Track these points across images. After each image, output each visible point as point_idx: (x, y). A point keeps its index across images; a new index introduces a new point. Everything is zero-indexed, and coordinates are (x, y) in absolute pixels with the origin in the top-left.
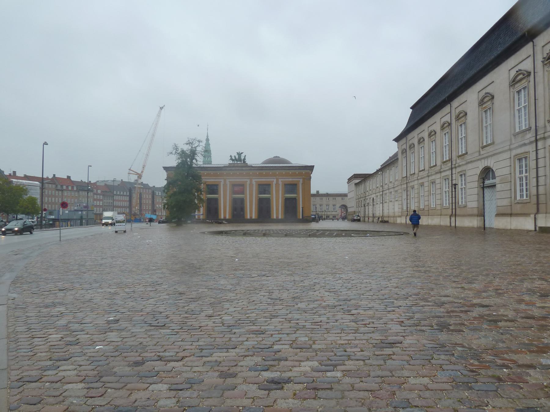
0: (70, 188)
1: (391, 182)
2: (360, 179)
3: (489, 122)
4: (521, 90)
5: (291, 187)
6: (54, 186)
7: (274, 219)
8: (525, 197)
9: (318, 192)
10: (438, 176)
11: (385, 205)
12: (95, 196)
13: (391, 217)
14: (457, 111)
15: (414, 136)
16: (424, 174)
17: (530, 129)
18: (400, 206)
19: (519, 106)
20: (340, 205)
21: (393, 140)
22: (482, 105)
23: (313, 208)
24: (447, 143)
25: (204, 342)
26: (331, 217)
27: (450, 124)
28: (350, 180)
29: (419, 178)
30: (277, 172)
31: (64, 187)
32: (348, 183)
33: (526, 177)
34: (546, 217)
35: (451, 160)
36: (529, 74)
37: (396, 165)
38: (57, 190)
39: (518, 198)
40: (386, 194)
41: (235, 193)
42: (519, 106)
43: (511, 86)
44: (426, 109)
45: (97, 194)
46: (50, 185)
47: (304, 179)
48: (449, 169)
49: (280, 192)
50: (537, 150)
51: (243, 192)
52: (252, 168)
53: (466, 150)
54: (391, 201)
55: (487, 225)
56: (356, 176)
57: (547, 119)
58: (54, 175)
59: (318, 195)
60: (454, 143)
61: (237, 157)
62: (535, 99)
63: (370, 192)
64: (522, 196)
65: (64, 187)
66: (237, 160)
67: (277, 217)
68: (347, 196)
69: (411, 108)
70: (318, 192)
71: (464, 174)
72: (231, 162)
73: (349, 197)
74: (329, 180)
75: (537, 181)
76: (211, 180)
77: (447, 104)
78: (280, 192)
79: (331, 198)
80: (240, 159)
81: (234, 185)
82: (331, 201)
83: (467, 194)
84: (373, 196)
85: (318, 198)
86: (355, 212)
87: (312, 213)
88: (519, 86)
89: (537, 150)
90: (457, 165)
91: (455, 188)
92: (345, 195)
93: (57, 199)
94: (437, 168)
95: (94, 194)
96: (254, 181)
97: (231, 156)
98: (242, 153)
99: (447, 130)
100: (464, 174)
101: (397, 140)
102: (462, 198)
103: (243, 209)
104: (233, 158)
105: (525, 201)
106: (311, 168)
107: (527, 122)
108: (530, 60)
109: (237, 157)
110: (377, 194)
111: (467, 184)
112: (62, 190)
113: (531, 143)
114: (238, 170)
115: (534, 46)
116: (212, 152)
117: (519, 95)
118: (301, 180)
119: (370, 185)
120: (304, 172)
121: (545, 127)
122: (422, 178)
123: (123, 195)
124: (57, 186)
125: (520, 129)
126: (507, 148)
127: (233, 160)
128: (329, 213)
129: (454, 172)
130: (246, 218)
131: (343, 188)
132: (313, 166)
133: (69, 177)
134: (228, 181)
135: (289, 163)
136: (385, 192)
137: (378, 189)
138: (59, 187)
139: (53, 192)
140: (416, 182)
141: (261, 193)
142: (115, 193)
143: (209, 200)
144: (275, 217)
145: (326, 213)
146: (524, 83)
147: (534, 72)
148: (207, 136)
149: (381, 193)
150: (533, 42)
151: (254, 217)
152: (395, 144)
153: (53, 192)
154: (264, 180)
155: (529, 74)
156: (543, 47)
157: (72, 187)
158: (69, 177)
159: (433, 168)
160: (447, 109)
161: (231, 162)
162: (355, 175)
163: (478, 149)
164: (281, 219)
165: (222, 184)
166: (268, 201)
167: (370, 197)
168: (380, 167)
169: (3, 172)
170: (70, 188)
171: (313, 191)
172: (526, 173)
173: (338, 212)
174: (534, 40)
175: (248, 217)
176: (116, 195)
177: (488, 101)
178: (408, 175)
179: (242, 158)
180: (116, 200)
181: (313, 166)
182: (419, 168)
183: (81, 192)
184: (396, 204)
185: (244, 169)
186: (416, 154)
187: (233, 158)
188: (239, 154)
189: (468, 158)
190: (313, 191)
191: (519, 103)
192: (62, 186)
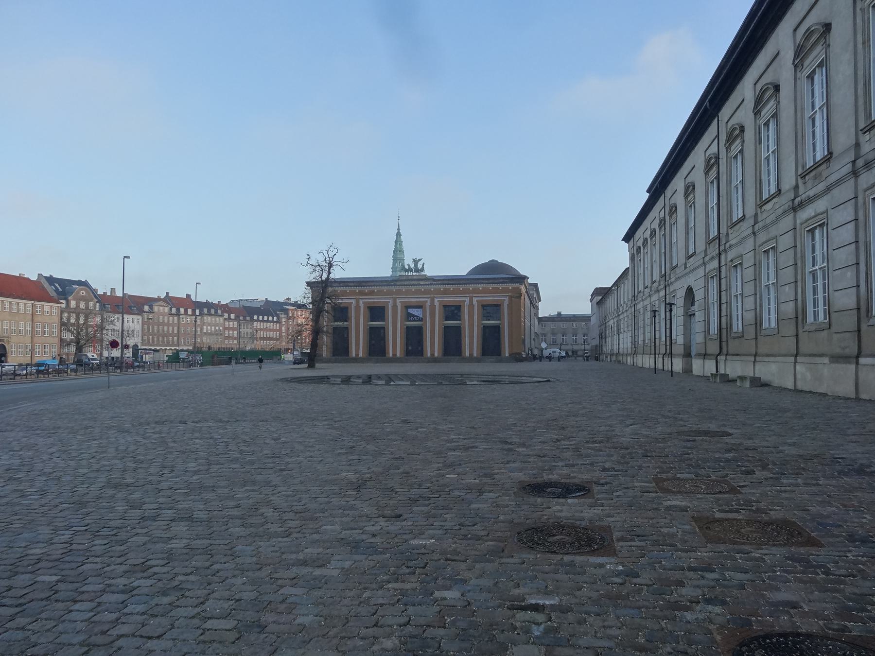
2: (601, 295)
11: (621, 336)
12: (227, 323)
25: (703, 577)
31: (182, 310)
32: (591, 300)
34: (726, 360)
35: (719, 237)
41: (487, 317)
47: (511, 298)
49: (476, 317)
51: (346, 319)
52: (433, 280)
58: (167, 293)
59: (559, 318)
61: (412, 266)
65: (182, 310)
78: (476, 317)
81: (484, 306)
91: (671, 310)
93: (171, 328)
96: (436, 300)
98: (420, 260)
101: (627, 238)
103: (420, 342)
109: (412, 266)
118: (507, 299)
128: (575, 347)
131: (585, 308)
136: (621, 317)
139: (166, 318)
141: (447, 319)
143: (335, 329)
148: (398, 229)
151: (475, 355)
153: (166, 318)
154: (450, 299)
162: (596, 289)
166: (458, 330)
169: (501, 283)
177: (768, 100)
183: (205, 318)
189: (678, 271)
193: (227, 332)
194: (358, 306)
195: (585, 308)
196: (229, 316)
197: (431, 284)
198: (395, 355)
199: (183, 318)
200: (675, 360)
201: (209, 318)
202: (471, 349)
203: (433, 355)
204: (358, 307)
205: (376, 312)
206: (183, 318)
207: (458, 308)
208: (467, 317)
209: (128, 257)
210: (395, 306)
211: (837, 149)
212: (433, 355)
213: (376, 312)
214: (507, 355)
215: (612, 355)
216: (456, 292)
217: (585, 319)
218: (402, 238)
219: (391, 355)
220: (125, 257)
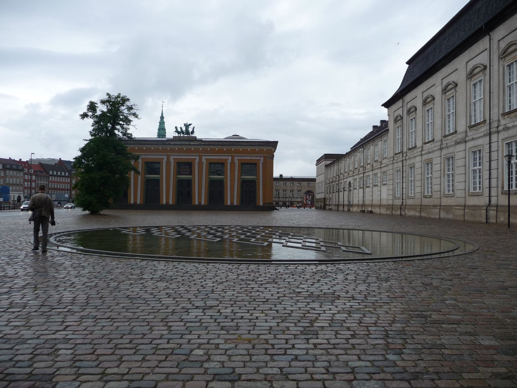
2: (330, 160)
3: (452, 111)
4: (512, 63)
5: (249, 167)
7: (228, 206)
8: (478, 190)
9: (281, 176)
10: (461, 147)
11: (367, 190)
12: (26, 176)
13: (376, 206)
14: (409, 107)
15: (416, 97)
16: (435, 146)
17: (485, 121)
18: (391, 192)
19: (510, 82)
20: (306, 191)
21: (383, 105)
22: (446, 93)
23: (275, 193)
24: (400, 136)
26: (281, 203)
27: (402, 118)
28: (319, 161)
29: (423, 152)
32: (317, 165)
33: (480, 170)
36: (485, 68)
37: (384, 138)
39: (472, 190)
40: (341, 183)
42: (510, 82)
43: (469, 78)
44: (425, 65)
47: (265, 158)
48: (485, 135)
49: (236, 173)
50: (490, 143)
53: (415, 144)
54: (377, 185)
55: (441, 217)
56: (327, 157)
57: (500, 113)
59: (281, 178)
60: (405, 137)
61: (184, 129)
62: (490, 92)
63: (346, 174)
64: (475, 189)
66: (183, 133)
67: (232, 203)
69: (407, 63)
70: (281, 176)
71: (431, 163)
72: (177, 135)
73: (317, 182)
75: (490, 174)
76: (152, 157)
77: (486, 35)
78: (236, 173)
79: (296, 183)
80: (187, 132)
83: (433, 183)
84: (349, 179)
85: (282, 183)
87: (274, 199)
88: (475, 80)
89: (490, 143)
90: (501, 128)
92: (313, 180)
94: (459, 137)
95: (25, 174)
97: (176, 128)
98: (190, 125)
99: (399, 123)
100: (452, 158)
101: (387, 105)
102: (428, 188)
104: (179, 130)
105: (479, 194)
107: (482, 115)
108: (486, 53)
109: (184, 129)
110: (355, 177)
111: (434, 173)
113: (485, 135)
115: (490, 39)
116: (166, 131)
117: (510, 69)
118: (262, 159)
119: (343, 165)
120: (265, 149)
121: (499, 120)
122: (429, 153)
123: (60, 176)
125: (510, 108)
126: (379, 166)
127: (179, 133)
128: (293, 200)
129: (404, 164)
130: (193, 204)
132: (277, 142)
133: (60, 159)
137: (356, 171)
140: (418, 159)
141: (213, 173)
142: (51, 173)
144: (229, 203)
145: (290, 200)
146: (480, 77)
147: (490, 65)
148: (162, 114)
149: (337, 182)
150: (490, 36)
151: (171, 202)
152: (385, 110)
155: (485, 68)
156: (499, 41)
159: (450, 137)
160: (483, 44)
161: (177, 135)
162: (325, 155)
163: (440, 139)
164: (140, 205)
167: (345, 180)
168: (350, 150)
171: (276, 175)
172: (480, 166)
174: (491, 34)
175: (229, 203)
176: (52, 176)
178: (405, 150)
179: (190, 130)
180: (68, 183)
181: (277, 142)
182: (423, 138)
183: (7, 172)
184: (384, 189)
185: (192, 143)
186: (419, 121)
187: (179, 130)
188: (187, 126)
190: (276, 175)
191: (510, 79)
193: (26, 183)
195: (384, 114)
197: (200, 145)
200: (500, 214)
201: (11, 172)
204: (168, 163)
205: (152, 167)
207: (223, 164)
208: (229, 172)
210: (168, 163)
211: (436, 140)
213: (217, 167)
214: (261, 204)
215: (344, 205)
216: (221, 152)
218: (165, 120)
219: (132, 202)
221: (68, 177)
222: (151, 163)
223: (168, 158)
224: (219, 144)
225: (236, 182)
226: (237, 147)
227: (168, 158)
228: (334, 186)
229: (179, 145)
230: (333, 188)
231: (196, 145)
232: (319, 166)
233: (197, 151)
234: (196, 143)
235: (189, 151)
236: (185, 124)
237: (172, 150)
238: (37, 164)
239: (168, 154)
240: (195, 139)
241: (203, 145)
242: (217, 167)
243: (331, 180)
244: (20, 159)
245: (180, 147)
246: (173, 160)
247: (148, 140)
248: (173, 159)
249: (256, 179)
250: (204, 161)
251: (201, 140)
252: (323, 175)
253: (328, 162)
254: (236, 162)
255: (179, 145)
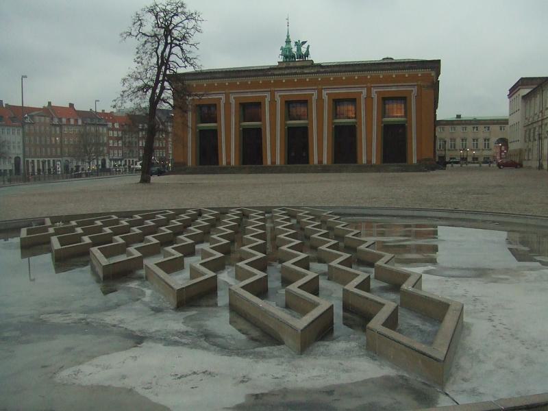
0: (72, 122)
1: (535, 115)
6: (48, 119)
7: (316, 166)
12: (111, 132)
28: (513, 90)
30: (369, 75)
31: (64, 120)
32: (510, 96)
38: (53, 125)
45: (113, 129)
46: (43, 119)
47: (420, 87)
49: (375, 113)
51: (214, 119)
56: (524, 82)
58: (50, 103)
59: (458, 122)
65: (64, 120)
68: (507, 124)
73: (511, 123)
74: (473, 91)
78: (375, 113)
79: (481, 128)
82: (482, 133)
85: (459, 128)
86: (521, 150)
92: (505, 122)
95: (109, 129)
98: (304, 43)
106: (435, 65)
112: (60, 126)
114: (296, 74)
118: (415, 90)
124: (52, 119)
131: (500, 107)
133: (71, 105)
134: (277, 95)
135: (392, 59)
138: (56, 121)
148: (288, 36)
149: (540, 123)
157: (76, 121)
158: (71, 105)
162: (522, 79)
165: (267, 100)
170: (72, 122)
173: (494, 151)
179: (304, 50)
192: (60, 119)
194: (227, 102)
196: (113, 125)
197: (318, 72)
198: (273, 163)
199: (66, 130)
202: (228, 156)
203: (320, 162)
204: (228, 104)
206: (66, 130)
207: (258, 105)
209: (98, 101)
210: (273, 102)
212: (320, 162)
213: (250, 110)
214: (415, 161)
216: (350, 81)
217: (503, 123)
219: (224, 163)
220: (23, 77)
221: (117, 130)
222: (408, 98)
223: (273, 96)
224: (348, 69)
225: (375, 127)
226: (374, 74)
227: (273, 96)
228: (535, 128)
229: (287, 74)
230: (534, 133)
231: (312, 73)
232: (513, 98)
233: (314, 82)
234: (313, 71)
235: (302, 83)
236: (296, 43)
237: (278, 84)
238: (124, 115)
239: (273, 89)
240: (312, 65)
241: (323, 73)
242: (250, 110)
243: (531, 120)
244: (459, 116)
245: (290, 77)
246: (279, 98)
247: (242, 71)
248: (280, 96)
249: (406, 121)
250: (325, 97)
251: (320, 66)
252: (519, 113)
253: (525, 91)
254: (374, 96)
255: (287, 74)
